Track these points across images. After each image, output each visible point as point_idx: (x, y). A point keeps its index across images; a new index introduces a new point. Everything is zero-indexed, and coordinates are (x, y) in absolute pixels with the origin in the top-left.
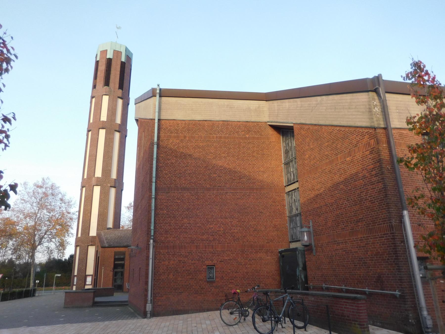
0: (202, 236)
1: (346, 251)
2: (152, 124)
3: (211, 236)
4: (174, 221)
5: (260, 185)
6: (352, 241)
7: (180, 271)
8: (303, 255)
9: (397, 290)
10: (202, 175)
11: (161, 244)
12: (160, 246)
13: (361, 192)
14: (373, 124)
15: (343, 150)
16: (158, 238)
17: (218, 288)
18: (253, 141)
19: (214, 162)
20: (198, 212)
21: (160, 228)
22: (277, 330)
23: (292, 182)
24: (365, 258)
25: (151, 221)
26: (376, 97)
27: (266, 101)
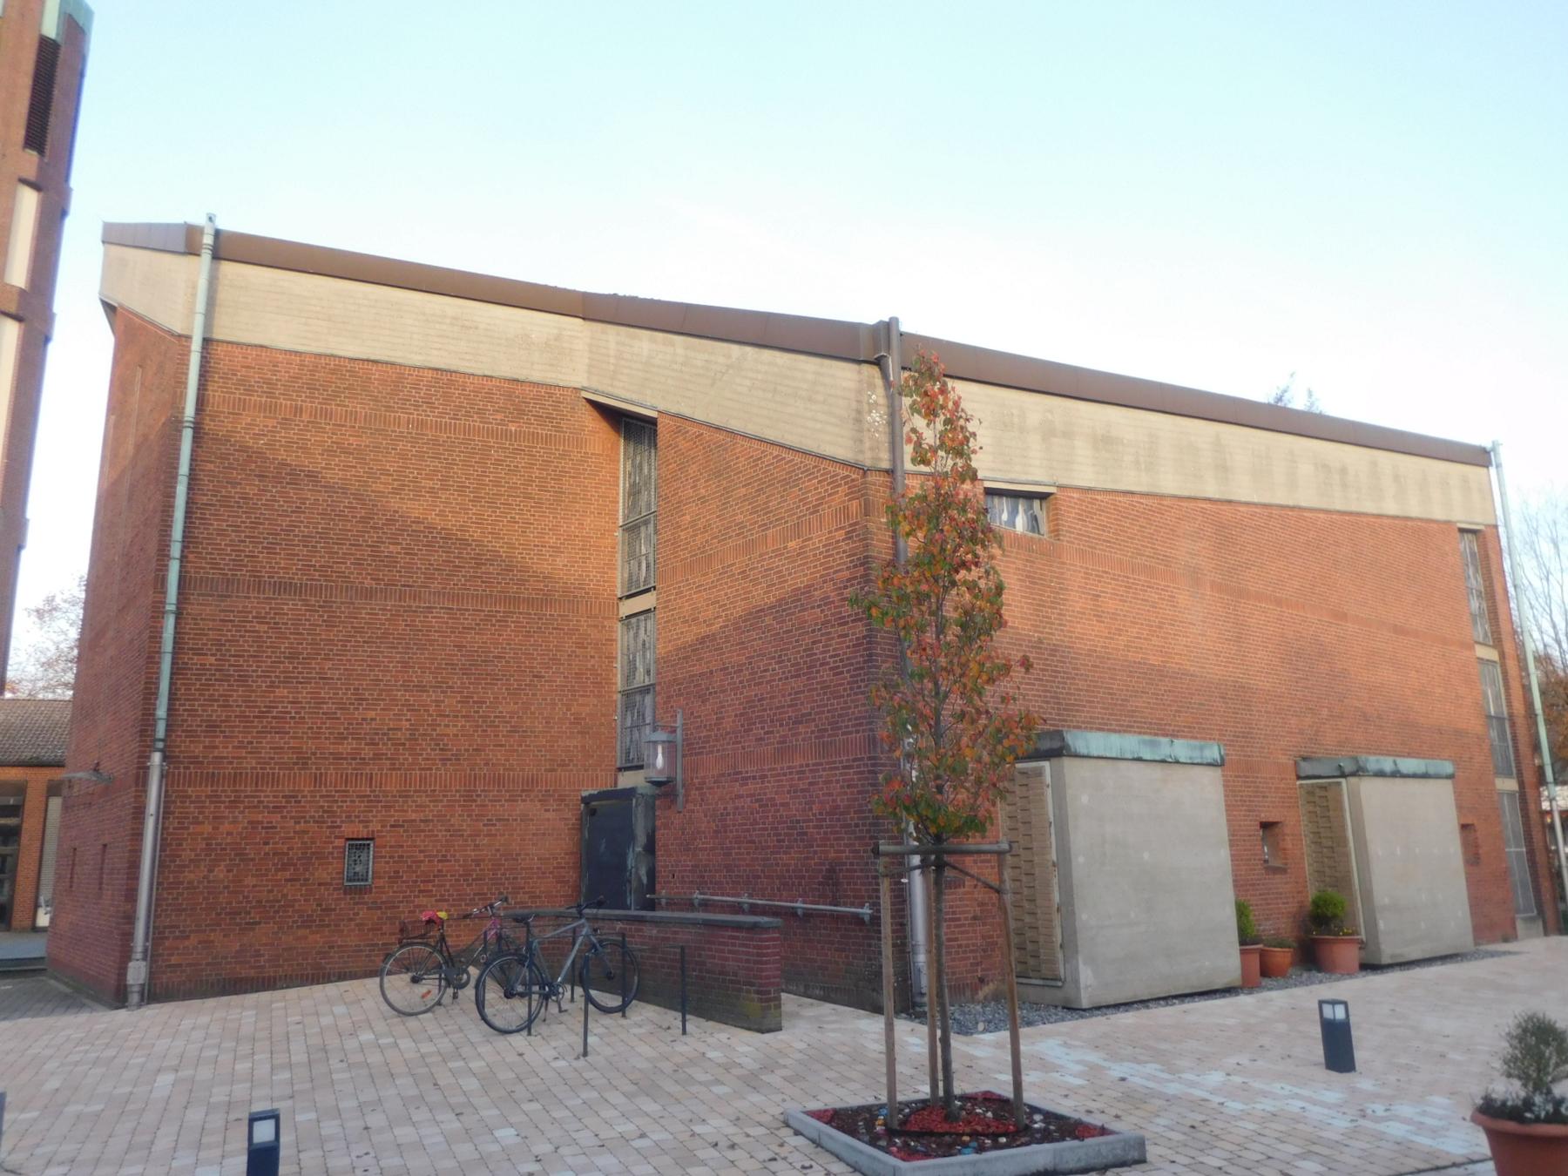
0: (339, 744)
1: (762, 800)
2: (180, 354)
3: (366, 744)
4: (243, 691)
5: (541, 590)
6: (779, 775)
7: (252, 856)
8: (651, 808)
9: (867, 904)
10: (350, 545)
11: (188, 768)
12: (185, 773)
13: (814, 643)
14: (860, 457)
15: (783, 518)
16: (180, 746)
17: (381, 908)
18: (530, 447)
19: (394, 503)
20: (329, 664)
21: (189, 715)
22: (544, 1020)
23: (642, 588)
24: (804, 821)
25: (158, 688)
26: (879, 382)
27: (584, 319)
